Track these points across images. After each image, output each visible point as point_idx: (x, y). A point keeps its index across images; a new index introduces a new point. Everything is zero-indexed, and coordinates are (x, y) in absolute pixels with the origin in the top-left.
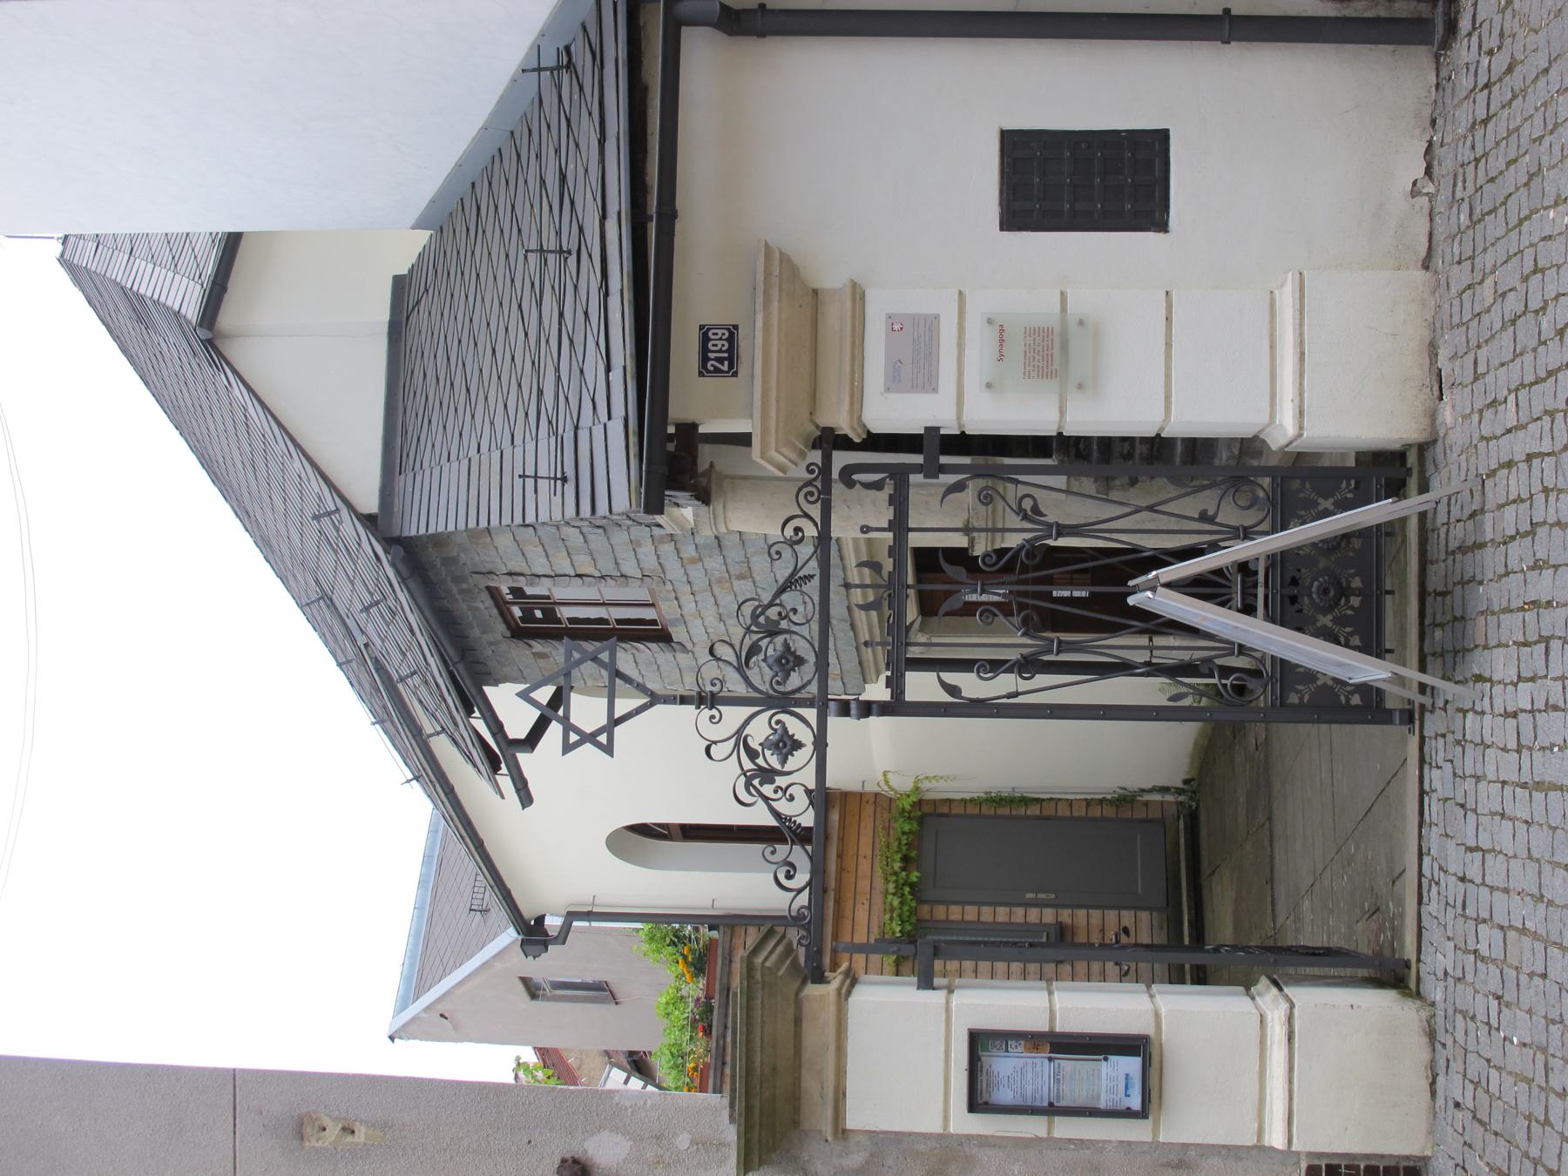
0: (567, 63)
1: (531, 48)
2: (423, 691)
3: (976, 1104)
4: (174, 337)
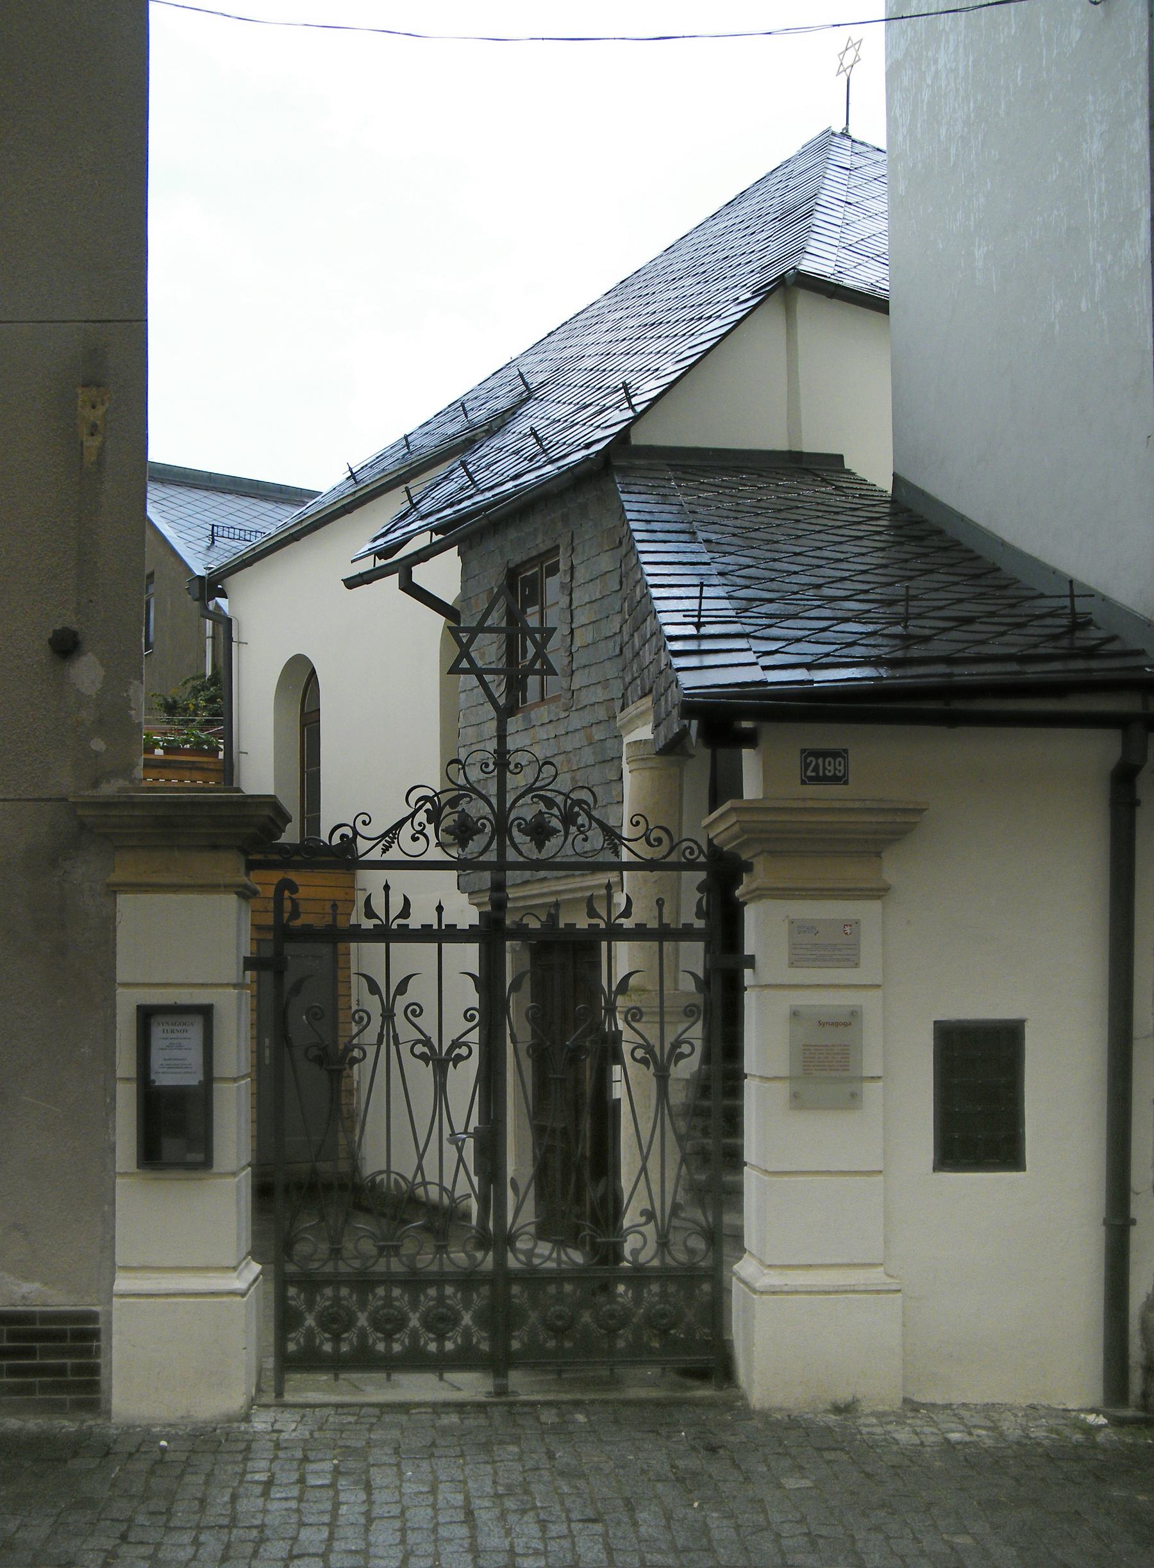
0: (1079, 623)
1: (1090, 589)
2: (452, 487)
3: (147, 1015)
4: (774, 250)
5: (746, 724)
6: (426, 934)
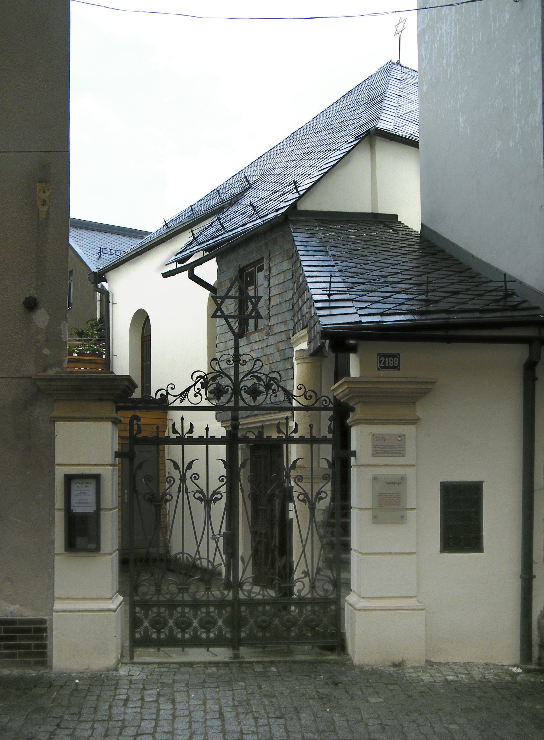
0: (509, 294)
1: (514, 278)
2: (213, 230)
3: (69, 479)
4: (365, 118)
5: (352, 342)
6: (201, 441)
